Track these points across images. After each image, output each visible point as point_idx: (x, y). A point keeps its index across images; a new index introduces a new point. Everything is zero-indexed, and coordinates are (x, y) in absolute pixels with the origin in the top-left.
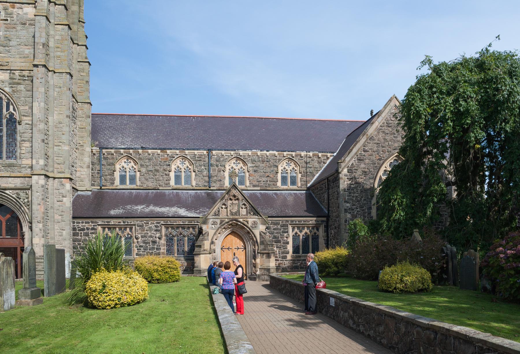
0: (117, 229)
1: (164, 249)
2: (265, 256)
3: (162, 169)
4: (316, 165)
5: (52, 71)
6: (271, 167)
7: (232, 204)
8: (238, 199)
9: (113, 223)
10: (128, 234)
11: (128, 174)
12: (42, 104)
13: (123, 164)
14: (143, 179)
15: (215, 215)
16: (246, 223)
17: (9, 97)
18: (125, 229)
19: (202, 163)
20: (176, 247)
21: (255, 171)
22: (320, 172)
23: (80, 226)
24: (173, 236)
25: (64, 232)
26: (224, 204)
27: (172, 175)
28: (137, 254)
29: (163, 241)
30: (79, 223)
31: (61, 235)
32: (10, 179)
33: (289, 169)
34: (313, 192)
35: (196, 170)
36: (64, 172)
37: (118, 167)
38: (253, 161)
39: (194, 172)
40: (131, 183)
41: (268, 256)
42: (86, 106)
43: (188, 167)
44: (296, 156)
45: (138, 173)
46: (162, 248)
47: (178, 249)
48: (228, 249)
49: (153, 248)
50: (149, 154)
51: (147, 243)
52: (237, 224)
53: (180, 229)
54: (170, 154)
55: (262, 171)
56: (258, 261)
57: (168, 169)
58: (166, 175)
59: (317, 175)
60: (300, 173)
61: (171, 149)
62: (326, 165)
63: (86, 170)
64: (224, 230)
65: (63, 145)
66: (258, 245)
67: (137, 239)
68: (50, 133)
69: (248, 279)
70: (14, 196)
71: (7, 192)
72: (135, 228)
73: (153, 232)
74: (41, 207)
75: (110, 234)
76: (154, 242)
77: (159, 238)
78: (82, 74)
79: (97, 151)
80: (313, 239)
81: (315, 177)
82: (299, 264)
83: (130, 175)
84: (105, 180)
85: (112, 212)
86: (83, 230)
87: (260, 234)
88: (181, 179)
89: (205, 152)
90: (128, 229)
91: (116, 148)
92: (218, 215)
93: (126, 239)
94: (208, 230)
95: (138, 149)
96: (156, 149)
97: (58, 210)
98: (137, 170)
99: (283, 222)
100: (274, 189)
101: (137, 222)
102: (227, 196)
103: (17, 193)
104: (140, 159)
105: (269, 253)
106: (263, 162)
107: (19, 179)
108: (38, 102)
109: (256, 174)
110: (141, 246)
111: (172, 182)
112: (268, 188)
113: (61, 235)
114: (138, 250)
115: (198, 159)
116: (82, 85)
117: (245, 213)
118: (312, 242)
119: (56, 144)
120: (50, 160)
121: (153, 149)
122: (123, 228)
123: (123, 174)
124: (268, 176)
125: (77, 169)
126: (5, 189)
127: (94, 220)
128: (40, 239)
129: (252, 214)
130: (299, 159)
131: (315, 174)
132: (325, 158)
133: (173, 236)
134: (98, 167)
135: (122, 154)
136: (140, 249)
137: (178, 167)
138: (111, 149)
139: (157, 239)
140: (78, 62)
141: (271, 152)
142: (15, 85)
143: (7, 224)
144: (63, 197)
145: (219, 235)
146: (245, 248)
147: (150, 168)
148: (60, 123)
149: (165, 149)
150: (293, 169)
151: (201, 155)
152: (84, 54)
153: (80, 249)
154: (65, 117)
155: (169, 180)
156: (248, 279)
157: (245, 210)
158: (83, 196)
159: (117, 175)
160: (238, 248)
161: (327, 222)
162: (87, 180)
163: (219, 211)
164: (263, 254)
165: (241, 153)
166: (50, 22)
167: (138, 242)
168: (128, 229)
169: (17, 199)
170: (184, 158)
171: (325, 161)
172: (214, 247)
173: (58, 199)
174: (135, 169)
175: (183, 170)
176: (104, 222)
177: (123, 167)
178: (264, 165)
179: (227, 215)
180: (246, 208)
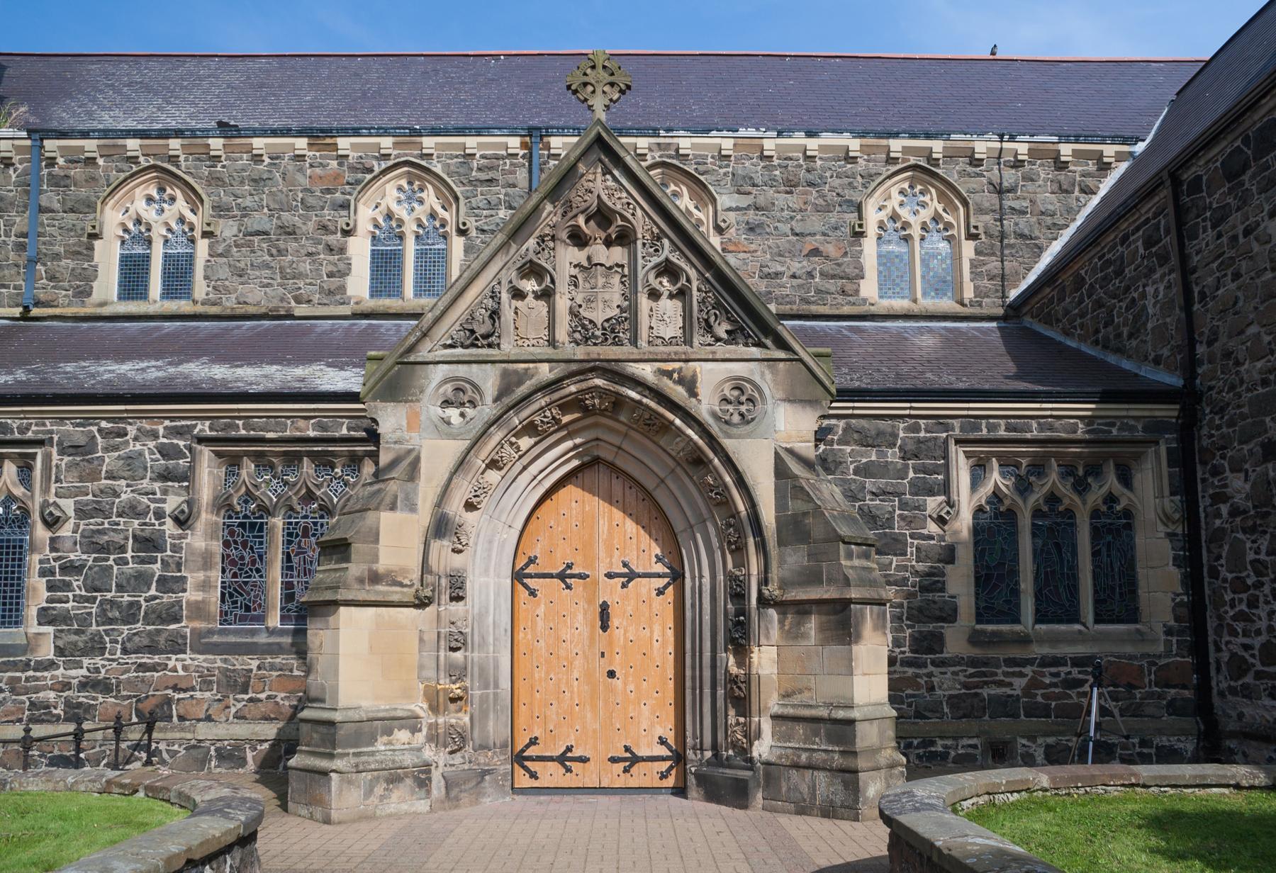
1: (205, 586)
2: (812, 625)
3: (311, 226)
4: (1048, 199)
6: (828, 209)
7: (589, 267)
8: (625, 238)
13: (140, 206)
14: (224, 272)
15: (472, 338)
16: (678, 393)
19: (500, 192)
20: (275, 574)
21: (751, 229)
22: (1066, 235)
24: (265, 510)
26: (532, 270)
27: (360, 250)
28: (46, 617)
29: (203, 539)
33: (916, 223)
34: (1048, 320)
35: (472, 224)
37: (112, 218)
38: (742, 185)
39: (462, 232)
40: (170, 292)
41: (840, 621)
43: (433, 215)
44: (950, 156)
45: (203, 246)
46: (193, 577)
47: (288, 586)
48: (562, 576)
49: (142, 580)
50: (257, 159)
51: (105, 549)
52: (619, 403)
53: (307, 467)
54: (353, 155)
55: (785, 228)
56: (765, 659)
57: (341, 223)
58: (330, 249)
59: (1056, 247)
60: (971, 237)
61: (356, 132)
62: (1095, 200)
64: (525, 442)
66: (762, 547)
67: (52, 522)
69: (694, 791)
73: (145, 484)
76: (149, 544)
77: (183, 521)
79: (19, 150)
80: (1096, 533)
81: (1046, 259)
82: (1019, 683)
83: (166, 256)
84: (52, 278)
87: (781, 471)
88: (400, 268)
89: (514, 142)
91: (105, 134)
92: (489, 339)
94: (415, 440)
95: (206, 133)
96: (285, 132)
99: (916, 429)
100: (846, 310)
101: (62, 426)
102: (550, 214)
104: (215, 181)
105: (846, 603)
106: (790, 185)
109: (757, 243)
111: (359, 285)
112: (815, 309)
114: (51, 587)
115: (483, 176)
117: (672, 329)
118: (1095, 554)
121: (275, 133)
123: (139, 250)
124: (815, 252)
129: (722, 329)
130: (962, 174)
131: (1042, 241)
132: (1092, 166)
133: (265, 510)
135: (134, 160)
136: (67, 586)
137: (389, 216)
138: (85, 135)
139: (169, 527)
141: (828, 139)
145: (493, 476)
146: (677, 576)
147: (260, 220)
149: (328, 132)
150: (936, 218)
151: (497, 158)
155: (344, 273)
156: (694, 791)
157: (671, 308)
159: (108, 256)
160: (631, 576)
161: (1188, 427)
163: (495, 314)
164: (802, 609)
165: (686, 143)
167: (54, 544)
170: (419, 171)
171: (1090, 182)
172: (457, 561)
175: (410, 228)
177: (138, 221)
178: (794, 201)
179: (552, 342)
180: (682, 294)
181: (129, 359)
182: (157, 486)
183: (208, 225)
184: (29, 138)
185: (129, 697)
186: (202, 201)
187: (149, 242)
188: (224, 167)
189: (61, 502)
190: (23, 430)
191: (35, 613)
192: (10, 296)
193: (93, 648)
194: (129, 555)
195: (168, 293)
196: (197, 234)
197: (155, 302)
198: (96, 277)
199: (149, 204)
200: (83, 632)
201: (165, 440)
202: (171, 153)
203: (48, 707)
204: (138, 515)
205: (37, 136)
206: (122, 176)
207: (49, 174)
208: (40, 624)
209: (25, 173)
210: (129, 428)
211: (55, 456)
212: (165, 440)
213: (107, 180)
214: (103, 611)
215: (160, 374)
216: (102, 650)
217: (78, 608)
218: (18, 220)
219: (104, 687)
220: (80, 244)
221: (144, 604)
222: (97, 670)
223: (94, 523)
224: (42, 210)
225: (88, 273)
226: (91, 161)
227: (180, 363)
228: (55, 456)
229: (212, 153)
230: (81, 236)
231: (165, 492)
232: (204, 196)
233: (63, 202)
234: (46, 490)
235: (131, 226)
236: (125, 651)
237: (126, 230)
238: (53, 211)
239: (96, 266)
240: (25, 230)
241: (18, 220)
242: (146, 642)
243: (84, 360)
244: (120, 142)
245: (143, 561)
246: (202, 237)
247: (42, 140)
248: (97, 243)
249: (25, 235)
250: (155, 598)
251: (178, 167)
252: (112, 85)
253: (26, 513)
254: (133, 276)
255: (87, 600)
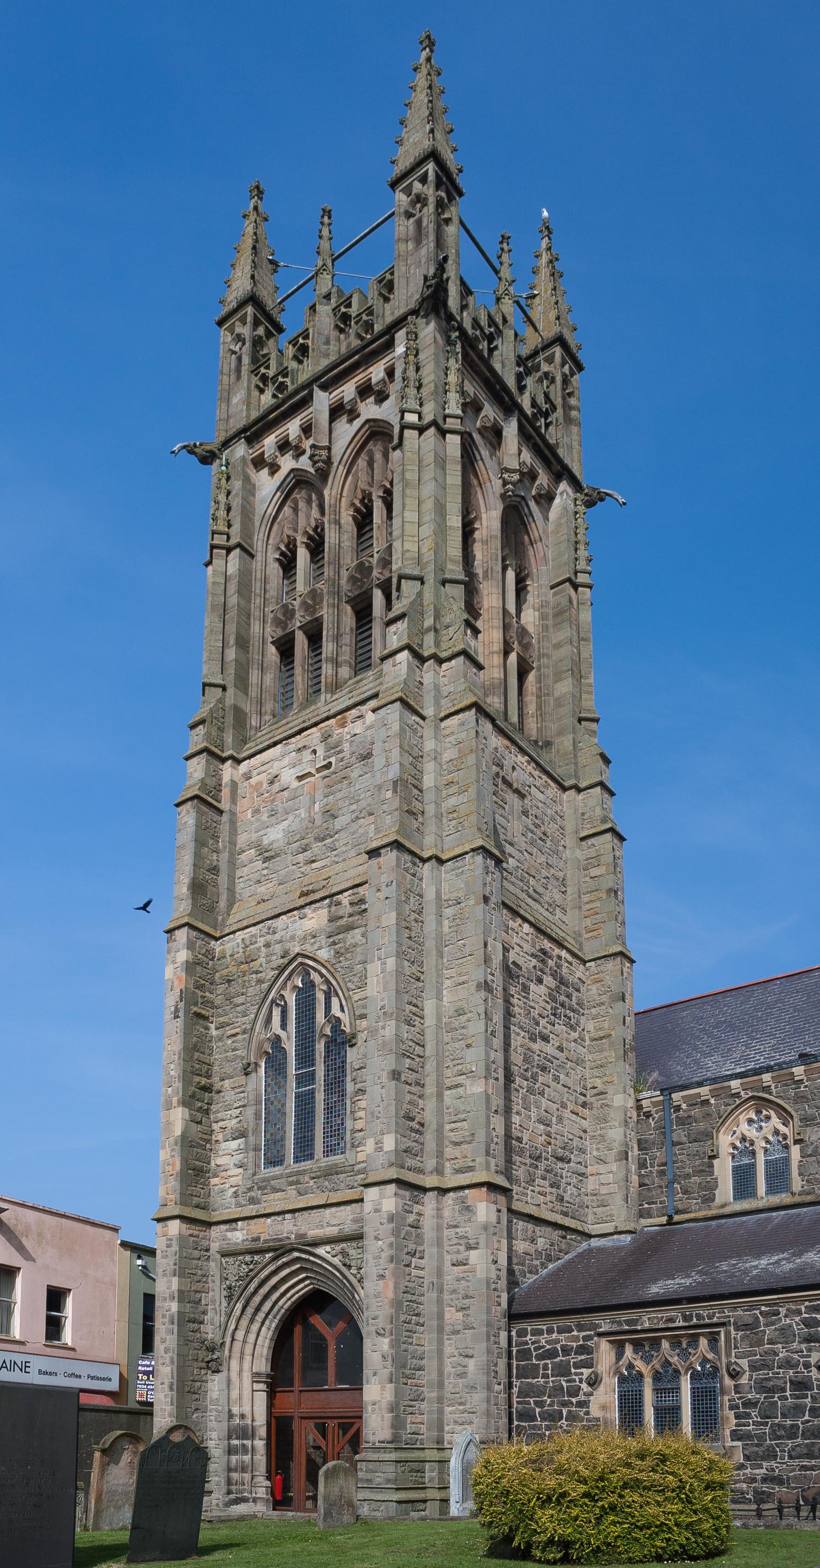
0: (665, 1345)
5: (430, 859)
9: (647, 1325)
10: (705, 1360)
11: (761, 1159)
12: (391, 962)
13: (744, 1128)
17: (328, 975)
18: (694, 1340)
23: (543, 1342)
25: (471, 1363)
28: (735, 1435)
30: (540, 1332)
31: (462, 1375)
32: (328, 1211)
36: (470, 1169)
37: (725, 1141)
42: (612, 966)
45: (795, 1151)
51: (771, 1390)
63: (614, 1167)
65: (468, 1082)
67: (734, 1375)
68: (430, 1050)
70: (336, 1261)
71: (321, 1251)
72: (728, 1334)
73: (795, 1345)
74: (386, 1286)
75: (640, 1365)
78: (594, 872)
79: (655, 1104)
83: (766, 1162)
84: (685, 1192)
85: (655, 1289)
86: (552, 1354)
90: (703, 1342)
91: (714, 1080)
93: (695, 1377)
95: (791, 1064)
97: (454, 1291)
98: (790, 1141)
103: (344, 1253)
107: (348, 1208)
108: (379, 959)
110: (749, 1404)
113: (462, 1375)
114: (737, 1417)
116: (597, 904)
119: (448, 1082)
120: (429, 1138)
122: (683, 1340)
123: (746, 1161)
125: (590, 1170)
126: (316, 1243)
127: (586, 1319)
128: (383, 1388)
134: (659, 1155)
135: (737, 1095)
136: (748, 1416)
138: (700, 1084)
140: (583, 839)
142: (340, 936)
143: (338, 1348)
144: (469, 1248)
148: (460, 1012)
152: (598, 810)
153: (543, 1419)
154: (473, 989)
158: (600, 1250)
159: (724, 1169)
162: (618, 1199)
166: (423, 718)
167: (737, 1389)
168: (703, 1342)
169: (343, 1269)
173: (455, 1257)
174: (785, 1137)
176: (620, 1323)
177: (744, 1139)
181: (764, 1254)
182: (803, 1346)
183: (799, 1134)
184: (662, 1095)
185: (797, 1488)
186: (792, 1117)
187: (753, 1153)
188: (806, 1087)
189: (739, 1361)
190: (710, 1317)
191: (729, 1434)
192: (658, 1209)
193: (769, 1455)
194: (788, 1393)
195: (771, 1190)
196: (790, 1141)
197: (762, 1198)
198: (717, 1186)
199: (749, 1125)
200: (761, 1445)
201: (807, 1316)
202: (764, 1085)
203: (743, 1493)
204: (792, 1367)
205: (667, 1093)
206: (730, 1108)
207: (677, 1117)
208: (732, 1440)
209: (660, 1120)
210: (781, 1309)
211: (733, 1332)
212: (807, 1316)
213: (719, 1114)
214: (773, 1432)
215: (791, 1266)
216: (775, 1457)
217: (757, 1430)
218: (658, 1154)
219: (779, 1481)
220: (703, 1164)
221: (801, 1426)
222: (773, 1470)
223: (761, 1374)
224: (675, 1144)
225: (711, 1184)
226: (706, 1102)
227: (800, 1255)
228: (733, 1332)
229: (796, 1078)
230: (704, 1158)
231: (809, 1350)
232: (793, 1113)
233: (689, 1136)
234: (728, 1355)
235: (738, 1144)
236: (791, 1457)
237: (735, 1147)
238: (681, 1144)
239: (716, 1179)
240: (664, 1161)
241: (658, 1154)
242: (805, 1451)
243: (731, 1258)
244: (726, 1084)
245: (798, 1397)
246: (795, 1144)
247: (670, 1094)
248: (716, 1162)
249: (665, 1164)
250: (809, 1421)
251: (770, 1094)
252: (704, 1029)
253: (716, 1369)
254: (744, 1180)
255: (762, 1424)
